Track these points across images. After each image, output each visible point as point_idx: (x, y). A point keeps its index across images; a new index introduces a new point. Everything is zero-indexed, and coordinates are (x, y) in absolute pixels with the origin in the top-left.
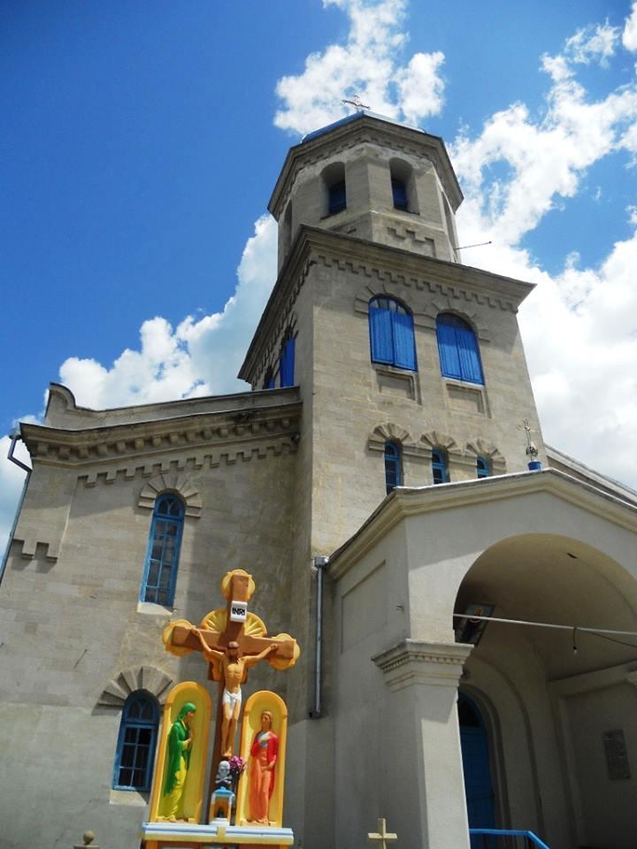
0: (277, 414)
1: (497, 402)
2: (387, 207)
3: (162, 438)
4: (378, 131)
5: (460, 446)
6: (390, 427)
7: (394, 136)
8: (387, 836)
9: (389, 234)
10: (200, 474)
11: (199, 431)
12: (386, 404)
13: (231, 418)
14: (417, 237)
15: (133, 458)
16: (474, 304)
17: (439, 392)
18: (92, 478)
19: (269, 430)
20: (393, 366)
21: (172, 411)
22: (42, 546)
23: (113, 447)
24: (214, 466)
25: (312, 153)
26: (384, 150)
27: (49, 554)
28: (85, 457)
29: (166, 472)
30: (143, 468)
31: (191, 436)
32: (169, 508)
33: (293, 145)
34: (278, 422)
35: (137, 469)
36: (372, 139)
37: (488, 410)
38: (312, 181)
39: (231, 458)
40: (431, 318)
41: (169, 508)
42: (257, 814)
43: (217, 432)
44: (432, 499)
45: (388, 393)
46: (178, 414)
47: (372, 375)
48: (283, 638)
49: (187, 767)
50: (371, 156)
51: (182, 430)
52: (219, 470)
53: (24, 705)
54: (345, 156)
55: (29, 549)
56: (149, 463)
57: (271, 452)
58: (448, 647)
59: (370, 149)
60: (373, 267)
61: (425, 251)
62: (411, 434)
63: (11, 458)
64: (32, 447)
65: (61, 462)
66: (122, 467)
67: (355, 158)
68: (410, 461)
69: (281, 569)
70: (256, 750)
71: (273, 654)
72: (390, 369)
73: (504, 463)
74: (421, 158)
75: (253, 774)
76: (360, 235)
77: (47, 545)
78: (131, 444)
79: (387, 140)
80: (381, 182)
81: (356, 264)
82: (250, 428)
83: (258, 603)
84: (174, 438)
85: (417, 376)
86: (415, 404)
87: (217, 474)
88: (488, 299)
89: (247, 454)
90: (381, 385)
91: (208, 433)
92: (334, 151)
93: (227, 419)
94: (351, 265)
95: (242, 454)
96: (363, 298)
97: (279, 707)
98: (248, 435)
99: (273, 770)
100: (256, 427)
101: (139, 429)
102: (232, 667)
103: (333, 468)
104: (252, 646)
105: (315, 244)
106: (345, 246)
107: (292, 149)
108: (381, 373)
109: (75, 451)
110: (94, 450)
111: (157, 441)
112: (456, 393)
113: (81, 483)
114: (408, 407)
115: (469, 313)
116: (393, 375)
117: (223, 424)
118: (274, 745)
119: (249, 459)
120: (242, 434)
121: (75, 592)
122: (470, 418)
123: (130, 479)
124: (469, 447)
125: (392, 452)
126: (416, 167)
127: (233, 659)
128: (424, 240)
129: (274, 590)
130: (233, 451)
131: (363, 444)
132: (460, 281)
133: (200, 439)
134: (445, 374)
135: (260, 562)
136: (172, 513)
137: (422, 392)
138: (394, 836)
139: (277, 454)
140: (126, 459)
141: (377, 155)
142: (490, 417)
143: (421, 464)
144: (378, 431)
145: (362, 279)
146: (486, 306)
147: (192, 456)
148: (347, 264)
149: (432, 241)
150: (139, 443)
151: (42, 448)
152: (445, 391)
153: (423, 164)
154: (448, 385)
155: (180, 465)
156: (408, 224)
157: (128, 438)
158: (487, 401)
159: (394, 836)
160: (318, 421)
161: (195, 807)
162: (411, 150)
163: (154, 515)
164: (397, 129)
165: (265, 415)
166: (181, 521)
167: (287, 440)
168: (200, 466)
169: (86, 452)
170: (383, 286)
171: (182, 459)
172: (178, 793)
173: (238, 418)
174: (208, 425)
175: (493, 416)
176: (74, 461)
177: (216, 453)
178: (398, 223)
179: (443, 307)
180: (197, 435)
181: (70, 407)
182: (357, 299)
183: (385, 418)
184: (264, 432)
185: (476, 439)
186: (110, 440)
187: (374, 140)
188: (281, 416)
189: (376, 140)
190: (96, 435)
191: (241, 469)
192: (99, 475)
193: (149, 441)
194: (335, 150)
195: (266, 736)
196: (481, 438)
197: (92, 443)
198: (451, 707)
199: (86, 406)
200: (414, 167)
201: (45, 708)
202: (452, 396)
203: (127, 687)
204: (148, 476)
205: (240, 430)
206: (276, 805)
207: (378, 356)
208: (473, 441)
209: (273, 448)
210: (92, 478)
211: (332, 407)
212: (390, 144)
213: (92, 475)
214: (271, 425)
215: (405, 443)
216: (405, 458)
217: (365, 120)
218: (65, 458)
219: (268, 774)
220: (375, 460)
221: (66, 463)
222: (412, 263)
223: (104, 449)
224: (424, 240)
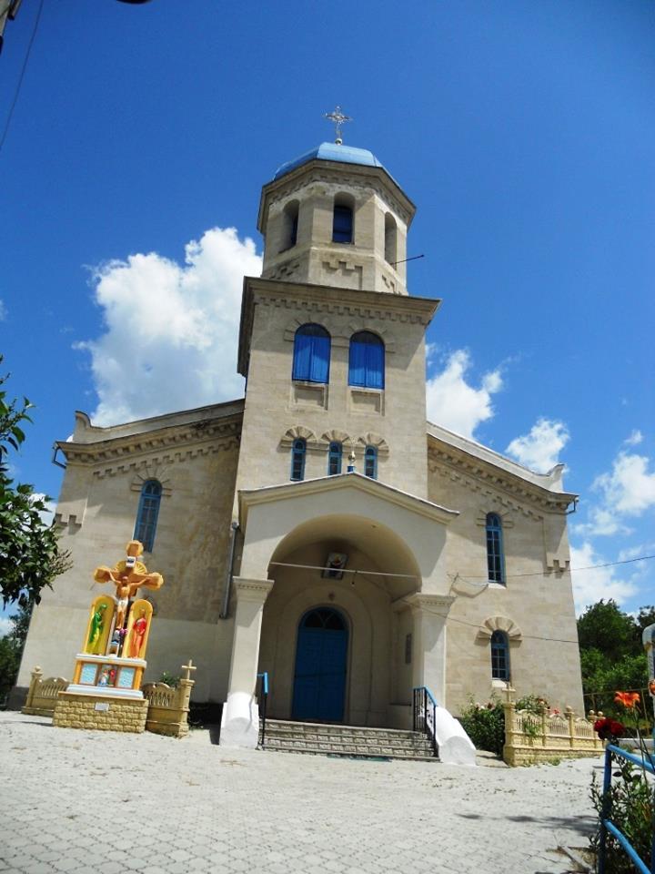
0: (227, 421)
1: (392, 401)
2: (324, 241)
3: (147, 444)
4: (327, 170)
5: (354, 442)
6: (298, 430)
7: (340, 171)
8: (191, 667)
9: (323, 267)
10: (173, 466)
11: (171, 437)
12: (300, 411)
13: (193, 427)
14: (348, 267)
15: (128, 458)
16: (388, 322)
17: (344, 398)
18: (102, 473)
19: (221, 432)
20: (309, 381)
21: (155, 424)
22: (73, 517)
23: (115, 452)
24: (182, 461)
25: (278, 190)
26: (332, 186)
27: (77, 522)
28: (97, 460)
29: (150, 466)
30: (135, 465)
31: (166, 441)
32: (153, 489)
33: (265, 183)
34: (227, 427)
35: (131, 465)
36: (322, 177)
37: (383, 410)
38: (277, 217)
39: (183, 456)
40: (345, 338)
41: (153, 489)
42: (133, 654)
43: (184, 437)
44: (266, 495)
45: (303, 403)
46: (159, 426)
47: (292, 391)
48: (155, 574)
49: (101, 633)
50: (319, 195)
51: (160, 438)
52: (185, 463)
53: (64, 608)
54: (300, 195)
55: (65, 519)
56: (138, 461)
57: (222, 448)
58: (262, 582)
59: (319, 188)
60: (302, 301)
61: (349, 283)
62: (315, 434)
63: (54, 462)
64: (66, 454)
65: (82, 464)
66: (121, 465)
67: (307, 196)
68: (312, 454)
69: (223, 528)
70: (135, 626)
71: (147, 582)
72: (306, 384)
73: (388, 451)
74: (364, 187)
75: (132, 637)
76: (295, 278)
77: (75, 517)
78: (126, 449)
79: (335, 176)
80: (323, 220)
81: (289, 300)
82: (208, 432)
83: (207, 549)
84: (155, 443)
85: (328, 388)
86: (322, 410)
87: (185, 465)
88: (400, 315)
89: (205, 450)
90: (297, 396)
91: (177, 438)
92: (295, 189)
93: (191, 427)
94: (285, 301)
95: (201, 450)
96: (290, 328)
97: (148, 608)
98: (206, 437)
99: (143, 635)
100: (211, 431)
101: (129, 440)
102: (124, 588)
103: (254, 462)
104: (137, 578)
105: (256, 289)
106: (280, 288)
107: (265, 186)
108: (298, 388)
109: (91, 456)
110: (102, 454)
111: (143, 446)
112: (359, 397)
113: (96, 477)
114: (316, 412)
115: (380, 331)
116: (309, 388)
117: (188, 431)
118: (144, 625)
119: (207, 454)
120: (202, 437)
121: (92, 544)
122: (366, 417)
123: (126, 472)
124: (360, 440)
125: (299, 448)
126: (358, 197)
127: (125, 585)
128: (354, 268)
129: (217, 541)
130: (195, 449)
131: (277, 443)
132: (375, 304)
133: (172, 442)
134: (351, 382)
135: (209, 523)
136: (154, 493)
137: (329, 399)
138: (195, 668)
139: (226, 449)
140: (123, 460)
141: (324, 193)
142: (383, 415)
143: (319, 455)
144: (289, 433)
145: (293, 313)
146: (398, 322)
147: (167, 454)
148: (282, 301)
149: (361, 268)
150: (132, 448)
151: (71, 456)
152: (350, 398)
153: (366, 193)
154: (352, 392)
155: (159, 461)
156: (342, 255)
157: (124, 445)
158: (384, 403)
159: (195, 668)
160: (246, 429)
161: (101, 648)
162: (355, 181)
163: (143, 495)
164: (343, 165)
165: (218, 423)
166: (160, 497)
167: (233, 438)
168: (172, 461)
169: (98, 457)
170: (309, 316)
171: (160, 457)
172: (94, 643)
173: (198, 426)
174: (177, 432)
175: (386, 414)
176: (91, 463)
177: (183, 451)
178: (333, 255)
179: (357, 328)
180: (170, 440)
181: (88, 427)
182: (287, 331)
183: (295, 423)
184: (196, 439)
185: (367, 433)
186: (112, 448)
187: (323, 178)
188: (229, 422)
189: (326, 177)
190: (102, 445)
191: (201, 462)
192: (107, 471)
193: (138, 446)
194: (294, 187)
195: (140, 621)
196: (371, 433)
197: (101, 451)
198: (254, 616)
199: (97, 426)
200: (357, 199)
201: (76, 610)
202: (355, 401)
203: (491, 629)
204: (138, 470)
205: (200, 434)
206: (143, 652)
207: (298, 375)
208: (365, 435)
209: (223, 445)
210: (102, 473)
211: (257, 417)
212: (337, 179)
213: (114, 468)
214: (222, 429)
215: (308, 441)
216: (307, 451)
217: (315, 162)
218: (84, 461)
219: (140, 638)
220: (285, 454)
221: (86, 464)
222: (334, 295)
223: (109, 454)
224: (354, 268)
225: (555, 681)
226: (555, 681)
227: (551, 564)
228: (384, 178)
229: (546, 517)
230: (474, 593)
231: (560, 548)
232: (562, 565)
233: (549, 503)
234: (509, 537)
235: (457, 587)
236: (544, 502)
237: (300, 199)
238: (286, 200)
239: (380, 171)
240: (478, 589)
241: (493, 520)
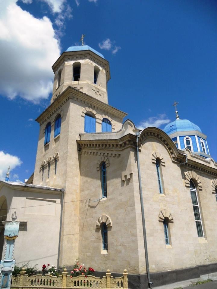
54: (82, 61)
189: (78, 57)
225: (125, 247)
226: (125, 247)
227: (123, 179)
228: (91, 53)
229: (121, 153)
230: (95, 206)
231: (127, 167)
232: (128, 177)
233: (121, 145)
234: (109, 170)
235: (91, 204)
236: (119, 146)
237: (81, 63)
238: (6, 182)
239: (89, 51)
240: (96, 203)
241: (103, 166)
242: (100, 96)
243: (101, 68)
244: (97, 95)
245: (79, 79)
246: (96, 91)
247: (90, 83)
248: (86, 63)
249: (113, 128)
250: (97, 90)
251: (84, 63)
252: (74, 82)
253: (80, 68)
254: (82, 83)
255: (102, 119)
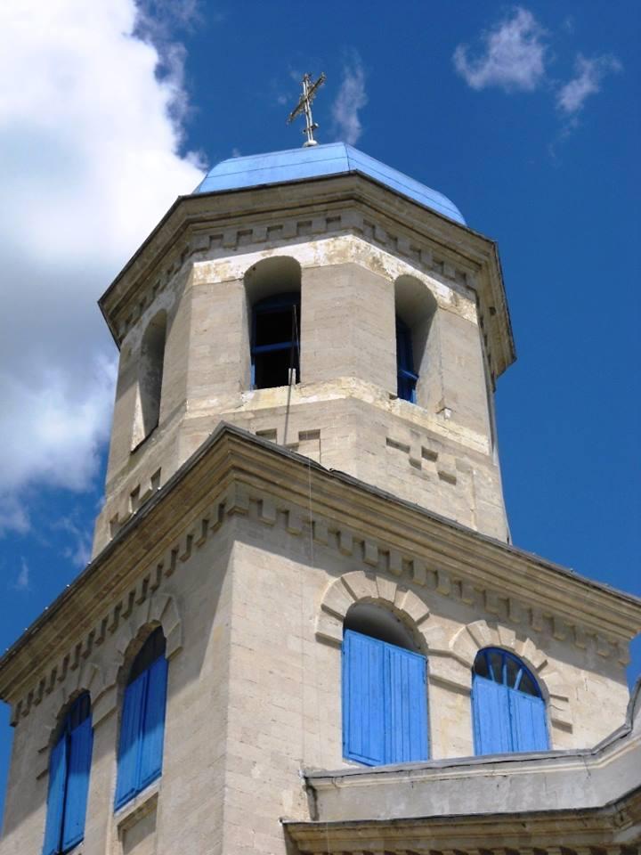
54: (306, 253)
242: (445, 484)
243: (441, 291)
244: (426, 477)
245: (292, 373)
246: (417, 455)
247: (369, 399)
248: (336, 262)
249: (561, 717)
250: (424, 442)
251: (323, 262)
252: (256, 399)
253: (294, 296)
254: (313, 399)
255: (470, 653)
